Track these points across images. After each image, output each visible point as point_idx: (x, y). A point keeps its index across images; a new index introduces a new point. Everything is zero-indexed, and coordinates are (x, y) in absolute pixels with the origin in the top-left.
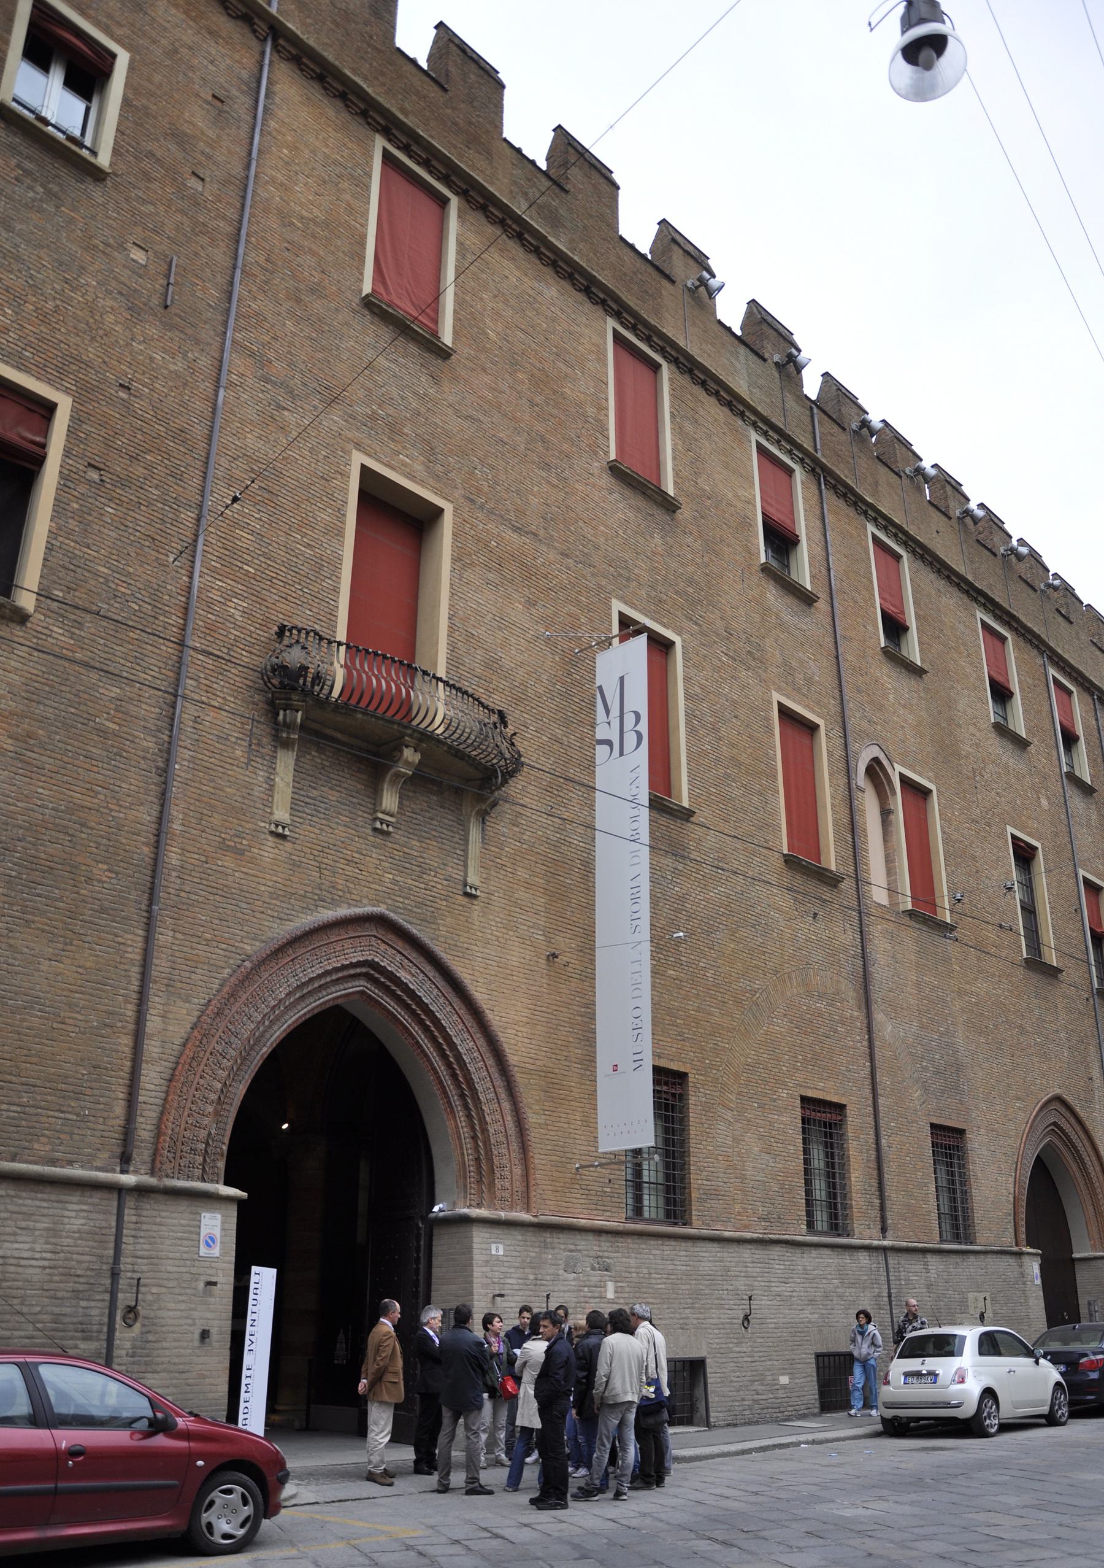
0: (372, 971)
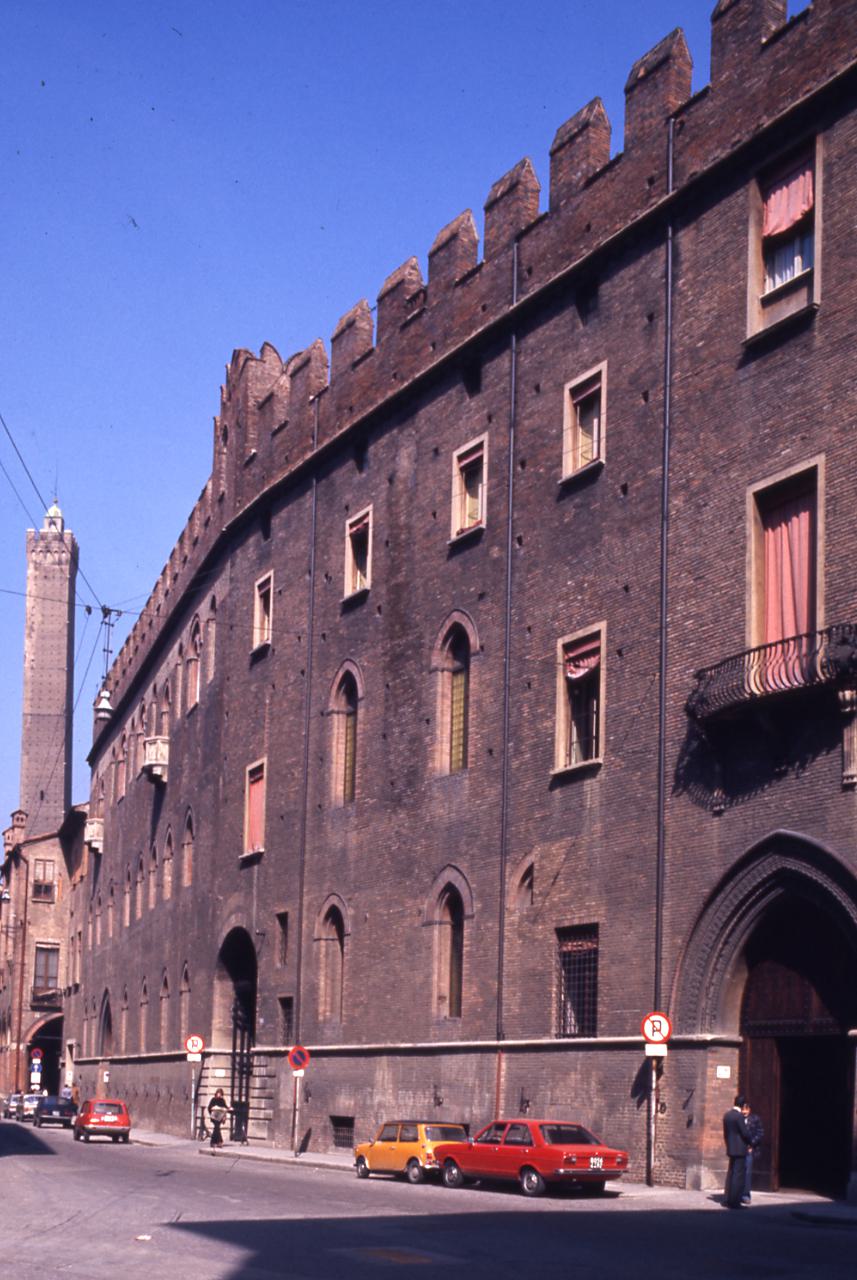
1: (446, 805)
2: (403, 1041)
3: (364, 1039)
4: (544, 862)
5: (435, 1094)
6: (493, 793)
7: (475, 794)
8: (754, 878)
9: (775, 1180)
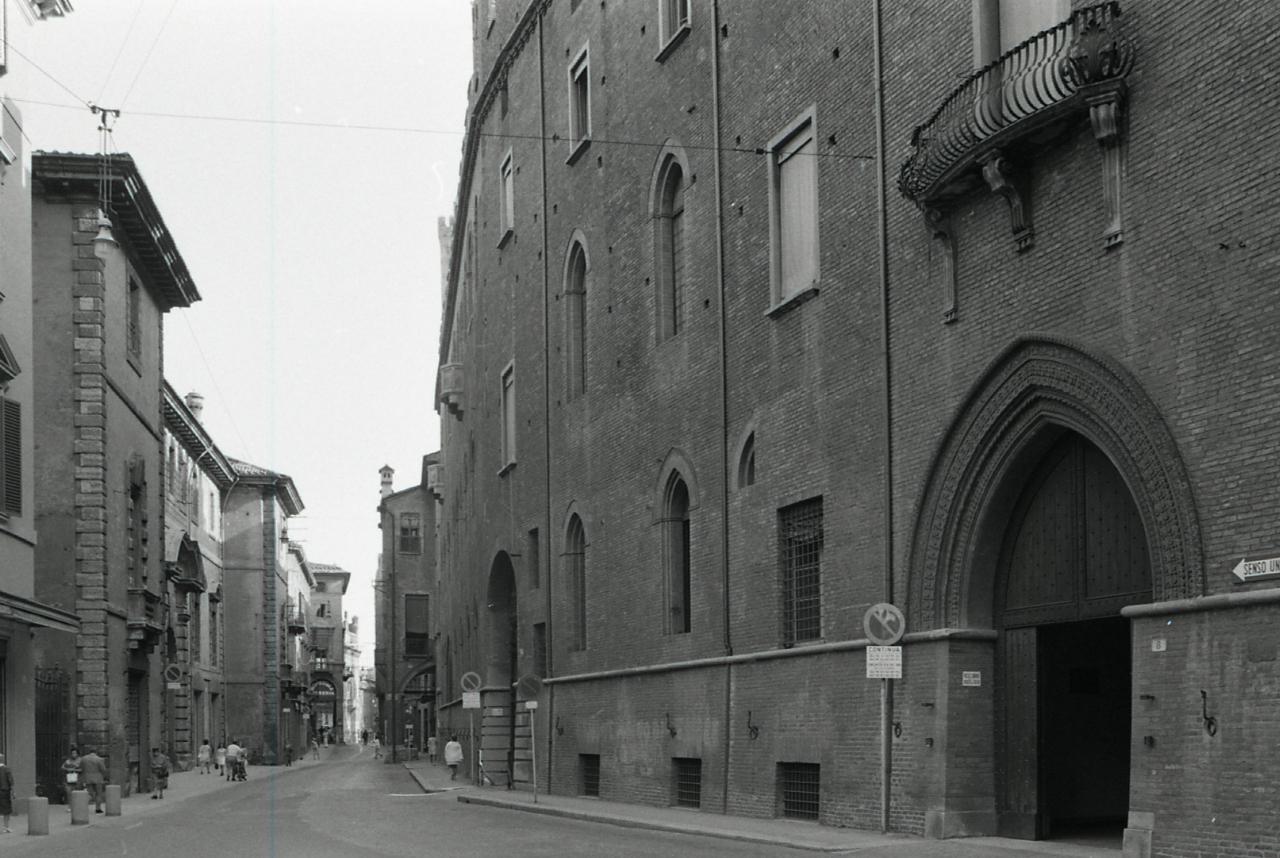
0: (1029, 398)
1: (668, 376)
2: (639, 665)
3: (606, 666)
4: (764, 428)
5: (668, 724)
6: (713, 353)
7: (695, 359)
8: (997, 407)
9: (1031, 827)
